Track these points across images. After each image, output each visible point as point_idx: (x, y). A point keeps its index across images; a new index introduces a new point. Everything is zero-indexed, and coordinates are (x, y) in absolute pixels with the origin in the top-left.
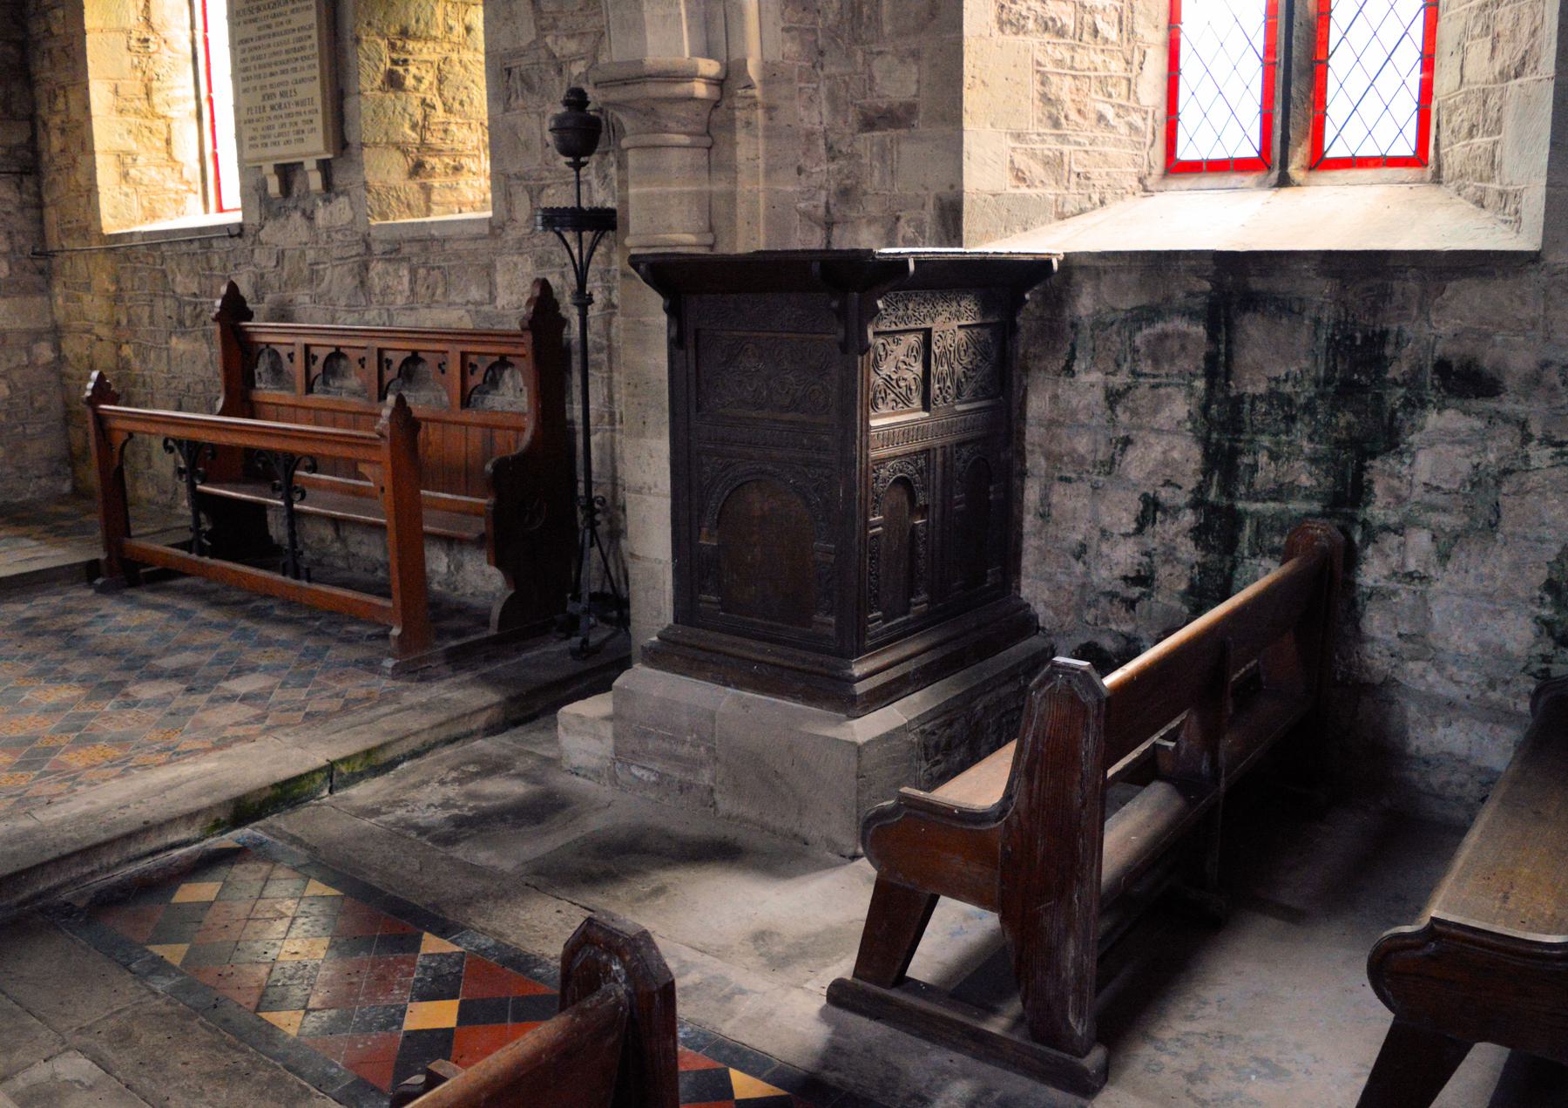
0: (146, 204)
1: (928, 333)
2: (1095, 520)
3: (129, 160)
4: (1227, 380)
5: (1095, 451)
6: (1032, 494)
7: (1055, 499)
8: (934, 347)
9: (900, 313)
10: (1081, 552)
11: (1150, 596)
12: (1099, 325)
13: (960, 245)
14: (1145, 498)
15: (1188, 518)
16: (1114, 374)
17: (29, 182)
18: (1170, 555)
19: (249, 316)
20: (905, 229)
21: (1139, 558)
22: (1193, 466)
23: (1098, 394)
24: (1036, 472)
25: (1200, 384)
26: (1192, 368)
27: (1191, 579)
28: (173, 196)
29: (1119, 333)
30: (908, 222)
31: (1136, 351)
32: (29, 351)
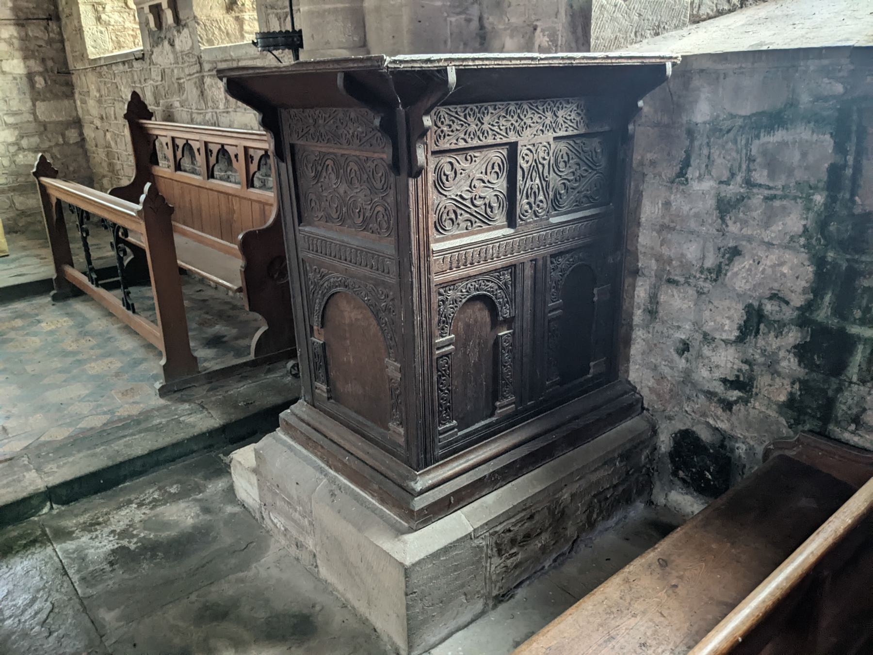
0: (114, 38)
1: (513, 148)
2: (697, 325)
3: (100, 9)
4: (853, 194)
5: (704, 258)
6: (641, 292)
7: (662, 298)
8: (520, 161)
9: (473, 128)
10: (684, 348)
11: (746, 402)
12: (716, 129)
13: (589, 51)
14: (749, 309)
15: (793, 337)
16: (727, 183)
17: (53, 25)
18: (772, 366)
19: (149, 115)
20: (541, 39)
21: (738, 364)
22: (804, 284)
23: (711, 203)
24: (646, 272)
25: (819, 198)
26: (813, 181)
27: (791, 393)
28: (131, 32)
29: (735, 142)
30: (543, 31)
31: (751, 160)
32: (63, 135)
